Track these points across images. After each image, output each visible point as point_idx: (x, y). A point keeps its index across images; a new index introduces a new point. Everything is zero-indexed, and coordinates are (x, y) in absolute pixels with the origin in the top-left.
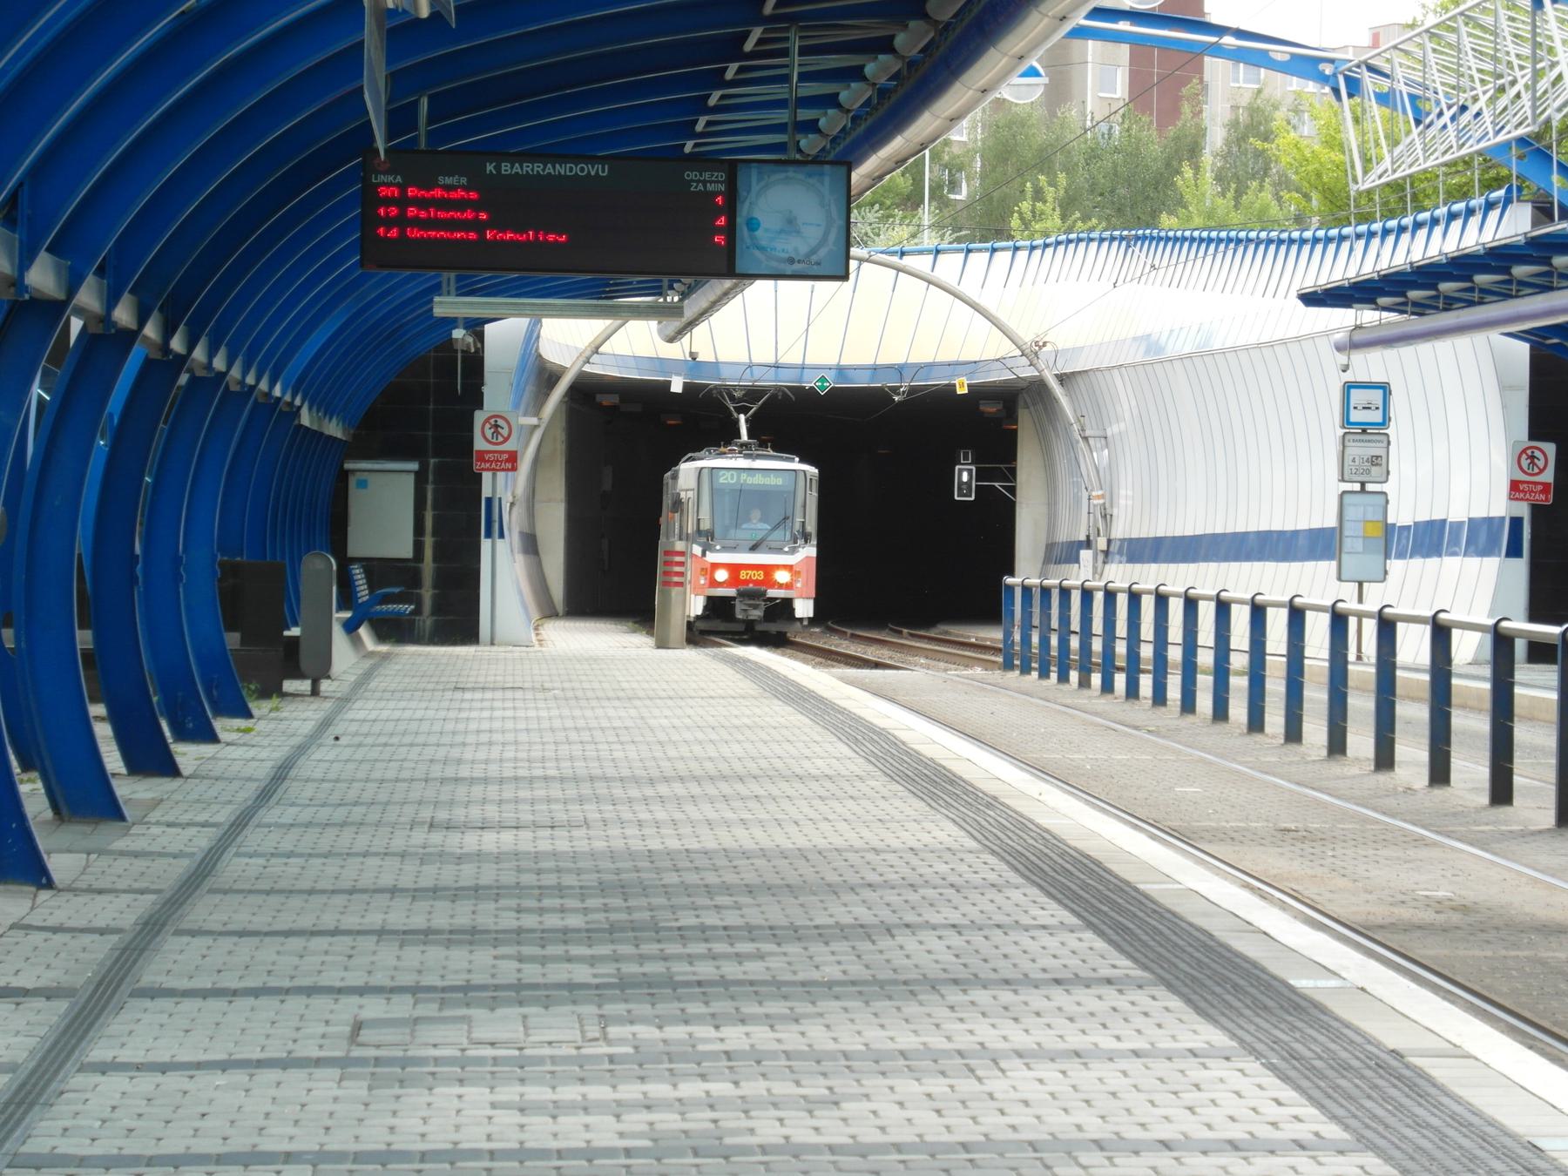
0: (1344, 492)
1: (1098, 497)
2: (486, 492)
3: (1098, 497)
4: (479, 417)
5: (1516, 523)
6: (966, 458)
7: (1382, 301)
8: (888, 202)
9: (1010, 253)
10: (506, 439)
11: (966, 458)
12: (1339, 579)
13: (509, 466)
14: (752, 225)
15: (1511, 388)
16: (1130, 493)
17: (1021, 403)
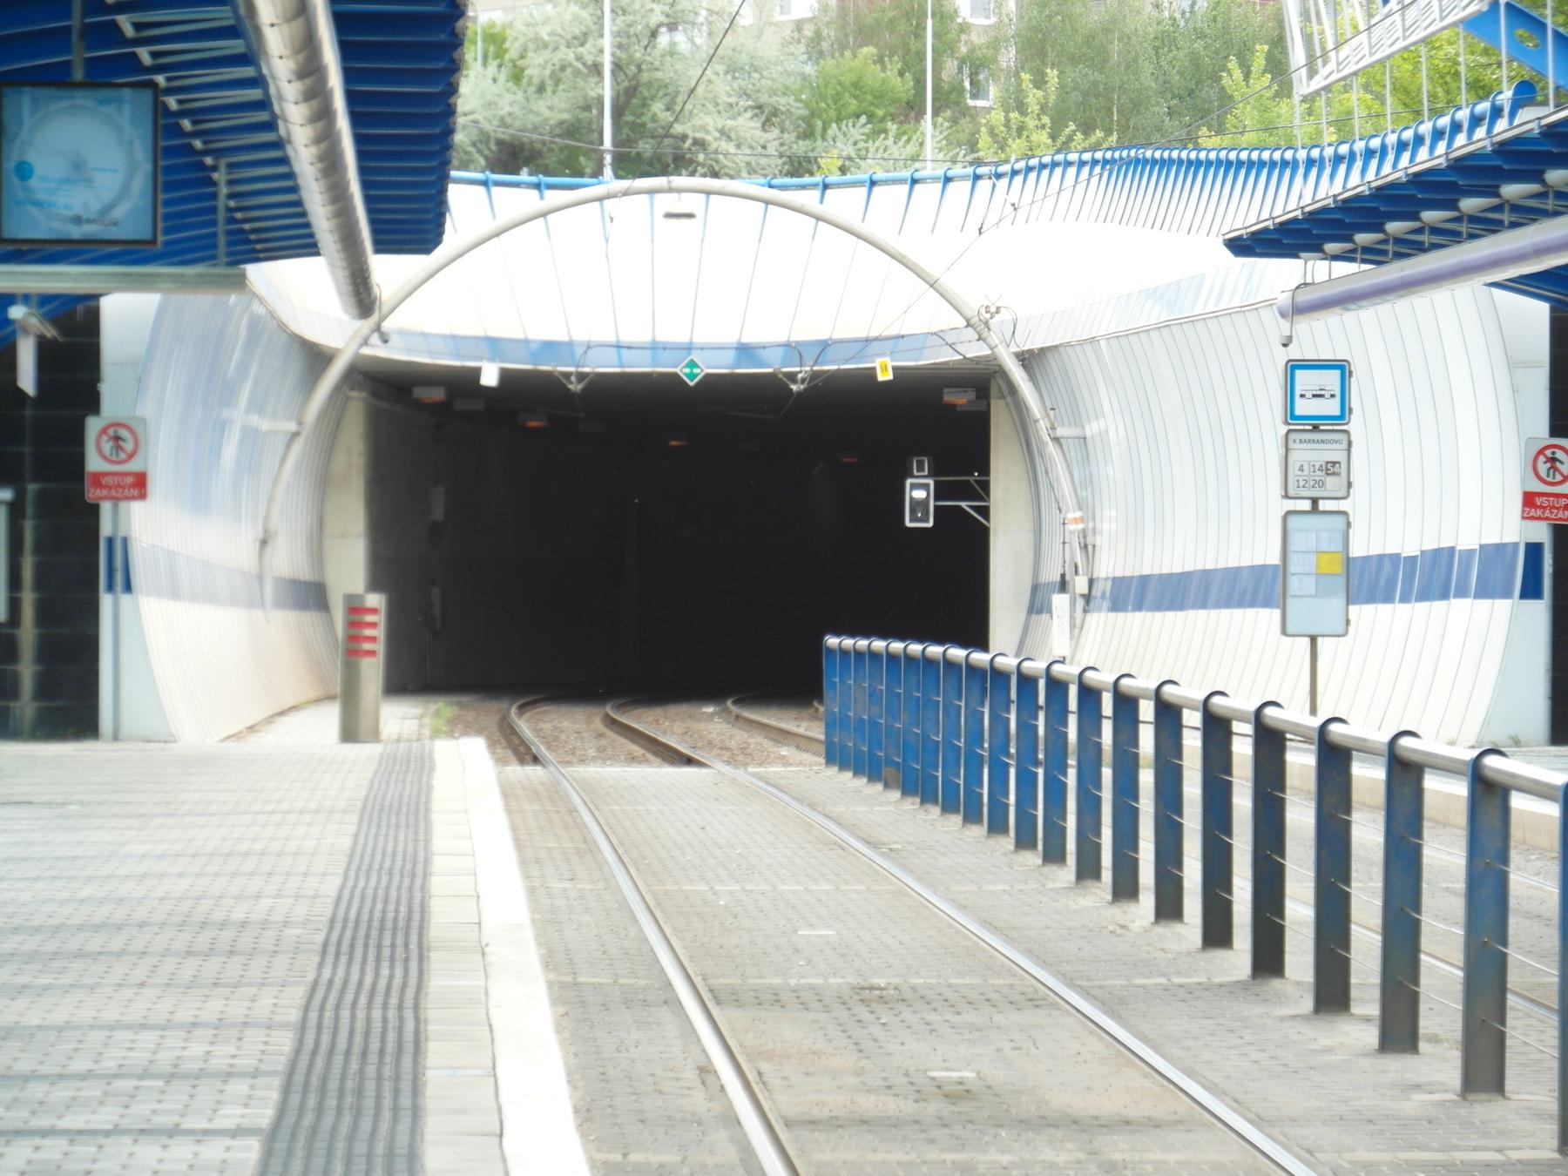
0: (1289, 513)
1: (1076, 521)
2: (106, 529)
3: (1076, 521)
4: (93, 425)
5: (1534, 550)
6: (920, 468)
7: (1331, 247)
8: (880, 113)
9: (969, 183)
10: (131, 456)
11: (920, 468)
12: (1284, 632)
13: (135, 492)
14: (24, 171)
15: (1525, 365)
16: (1114, 513)
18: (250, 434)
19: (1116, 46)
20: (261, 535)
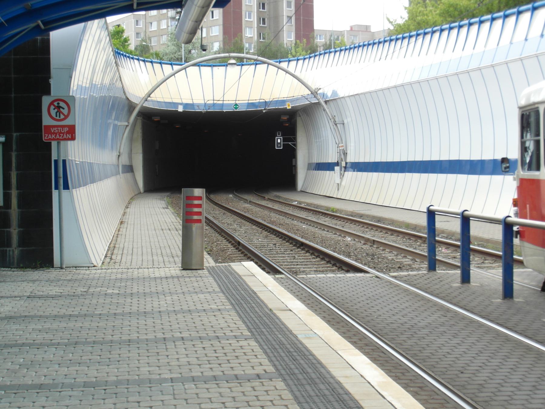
4: (46, 101)
6: (279, 134)
9: (296, 62)
10: (66, 117)
11: (279, 134)
17: (298, 115)
18: (115, 126)
19: (279, 54)
20: (118, 154)
